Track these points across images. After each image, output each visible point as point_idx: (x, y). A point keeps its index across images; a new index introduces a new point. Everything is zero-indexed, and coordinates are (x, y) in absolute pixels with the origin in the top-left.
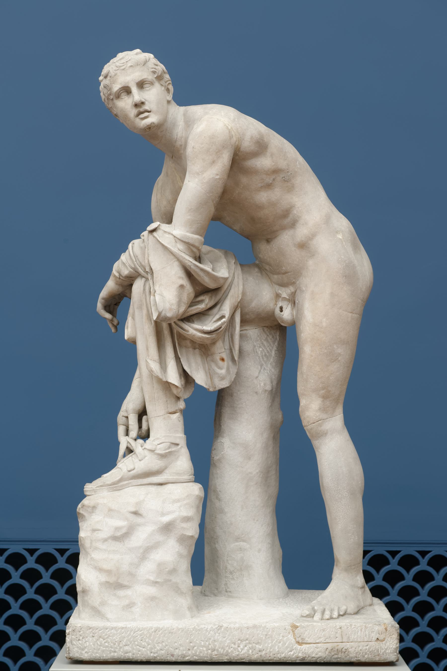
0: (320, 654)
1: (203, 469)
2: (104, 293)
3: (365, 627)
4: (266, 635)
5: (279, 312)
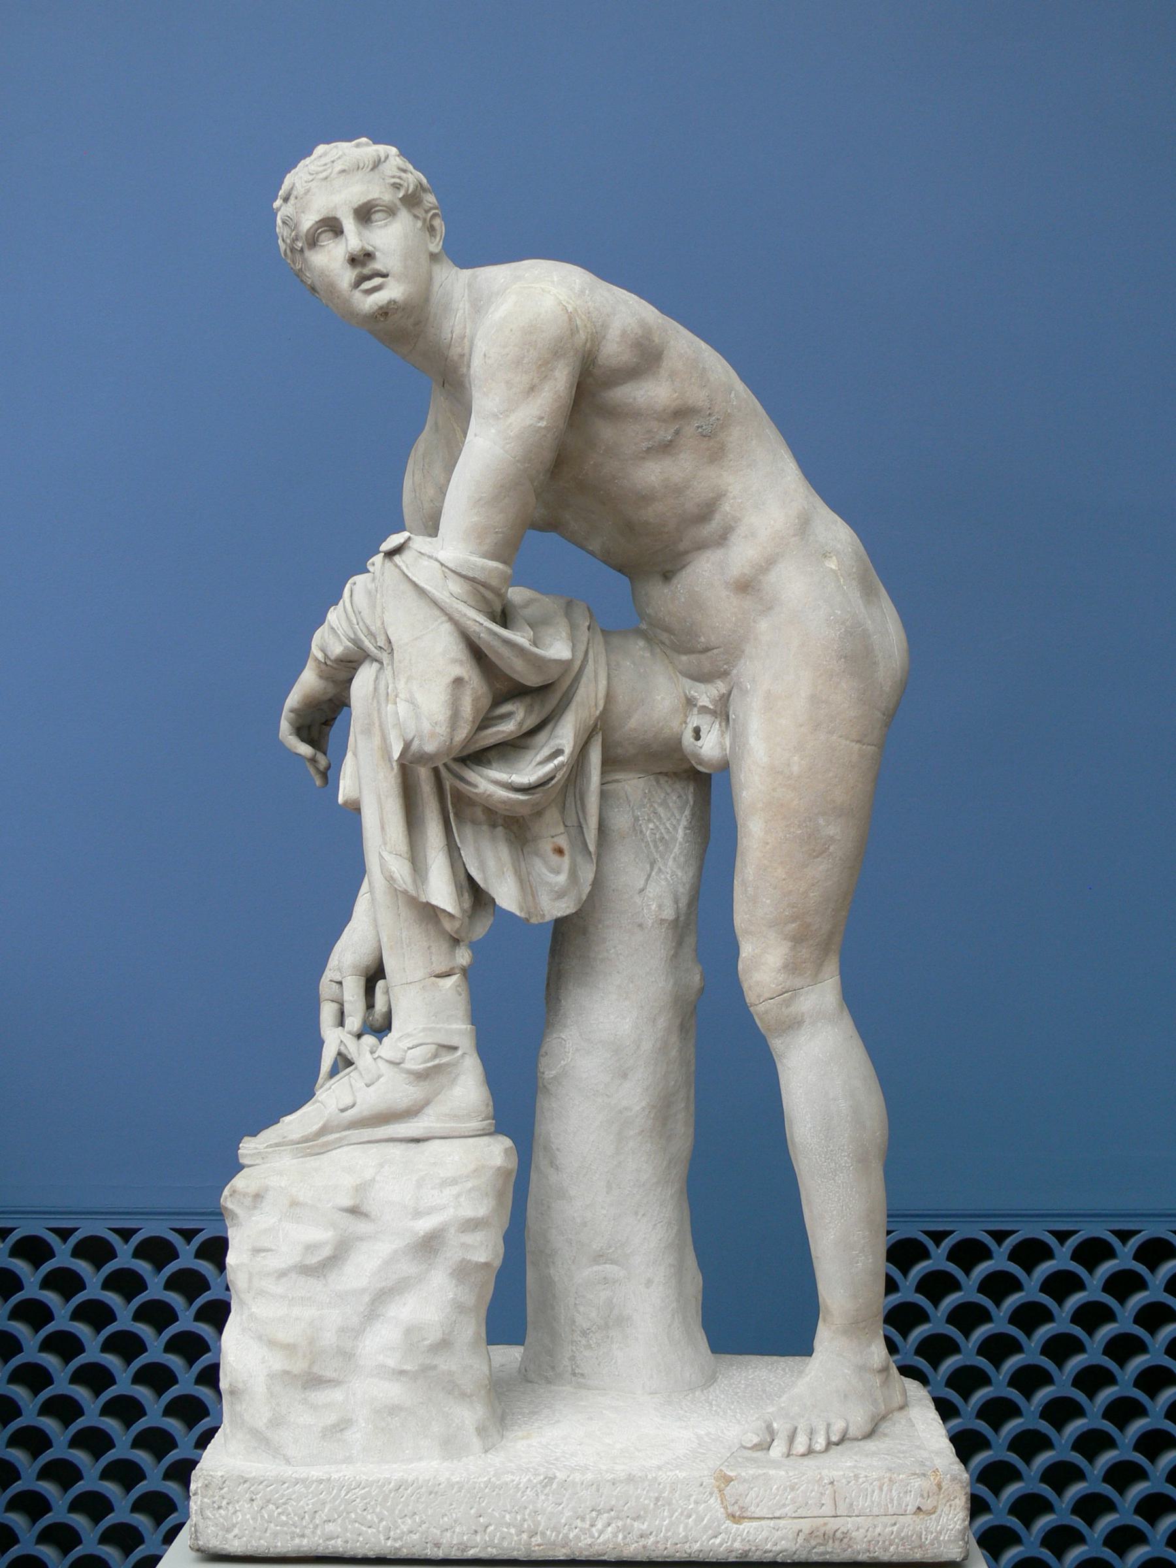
0: (783, 1544)
1: (516, 1106)
2: (293, 699)
3: (890, 1480)
4: (657, 1499)
5: (692, 740)
